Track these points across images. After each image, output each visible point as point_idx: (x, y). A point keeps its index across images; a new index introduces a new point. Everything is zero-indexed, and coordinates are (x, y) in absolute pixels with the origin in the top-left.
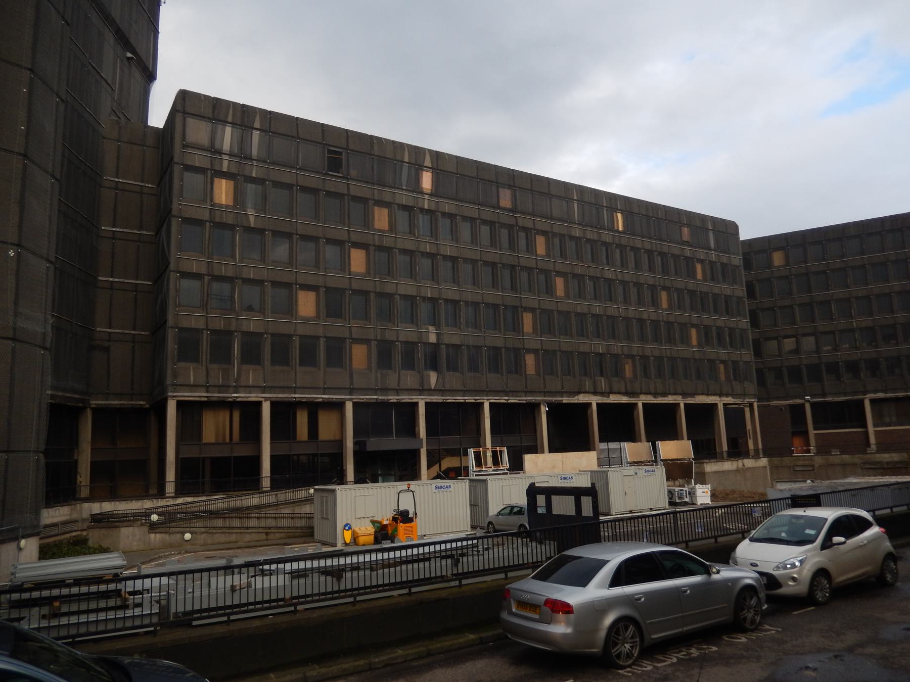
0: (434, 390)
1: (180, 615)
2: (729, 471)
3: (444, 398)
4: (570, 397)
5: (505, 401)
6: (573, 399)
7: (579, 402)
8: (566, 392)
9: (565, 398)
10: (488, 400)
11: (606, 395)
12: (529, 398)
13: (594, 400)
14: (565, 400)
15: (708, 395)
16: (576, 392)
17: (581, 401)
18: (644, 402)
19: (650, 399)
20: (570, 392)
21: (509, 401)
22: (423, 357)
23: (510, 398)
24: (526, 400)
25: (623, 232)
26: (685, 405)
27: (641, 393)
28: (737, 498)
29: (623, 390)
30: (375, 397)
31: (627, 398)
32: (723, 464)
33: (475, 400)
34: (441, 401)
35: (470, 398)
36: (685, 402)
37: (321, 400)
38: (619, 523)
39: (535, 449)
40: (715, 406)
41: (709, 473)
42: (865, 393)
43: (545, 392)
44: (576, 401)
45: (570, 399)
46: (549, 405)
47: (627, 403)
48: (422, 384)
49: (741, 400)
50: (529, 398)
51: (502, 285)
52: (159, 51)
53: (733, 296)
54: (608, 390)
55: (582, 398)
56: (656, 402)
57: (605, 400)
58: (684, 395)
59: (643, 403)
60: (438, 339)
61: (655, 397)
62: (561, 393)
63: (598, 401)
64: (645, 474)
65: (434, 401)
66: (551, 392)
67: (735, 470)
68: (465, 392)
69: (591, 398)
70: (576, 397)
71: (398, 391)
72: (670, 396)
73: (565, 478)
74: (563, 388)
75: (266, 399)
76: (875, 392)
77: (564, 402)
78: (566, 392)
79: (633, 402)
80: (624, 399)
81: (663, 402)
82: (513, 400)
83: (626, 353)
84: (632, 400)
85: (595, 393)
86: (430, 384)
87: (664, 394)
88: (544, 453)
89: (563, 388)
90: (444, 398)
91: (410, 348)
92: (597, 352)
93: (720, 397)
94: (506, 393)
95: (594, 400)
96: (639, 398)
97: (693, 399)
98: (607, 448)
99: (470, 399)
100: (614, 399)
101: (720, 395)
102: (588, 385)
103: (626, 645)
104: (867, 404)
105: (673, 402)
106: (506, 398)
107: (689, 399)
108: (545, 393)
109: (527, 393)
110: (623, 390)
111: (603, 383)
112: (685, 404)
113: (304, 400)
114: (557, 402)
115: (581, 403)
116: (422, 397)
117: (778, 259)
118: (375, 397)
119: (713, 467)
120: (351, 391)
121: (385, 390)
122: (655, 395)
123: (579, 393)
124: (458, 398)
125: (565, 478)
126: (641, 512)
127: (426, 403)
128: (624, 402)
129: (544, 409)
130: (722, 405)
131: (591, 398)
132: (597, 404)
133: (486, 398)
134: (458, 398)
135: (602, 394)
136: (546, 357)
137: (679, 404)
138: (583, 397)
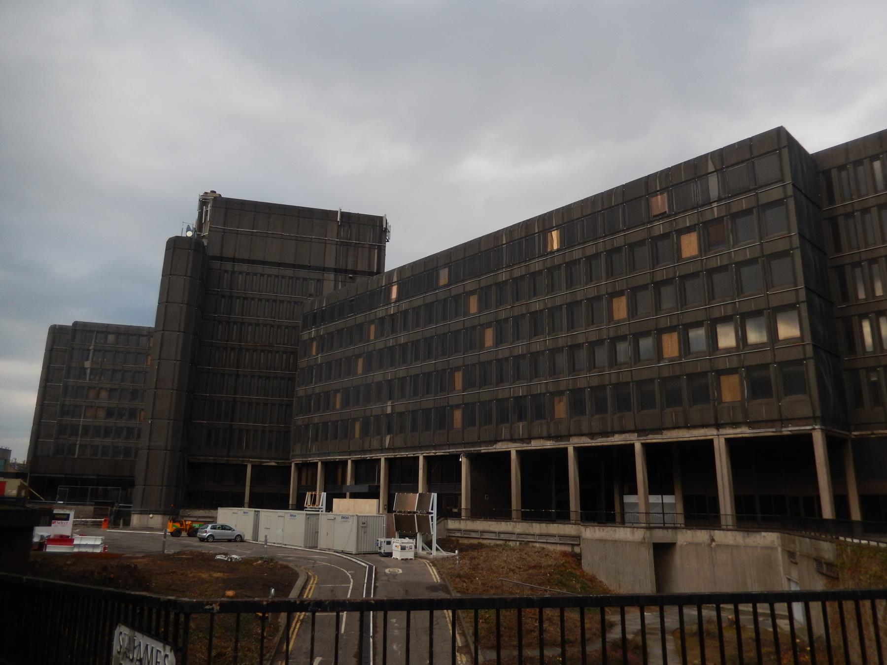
0: (388, 449)
1: (279, 566)
2: (624, 542)
3: (394, 454)
4: (488, 446)
5: (433, 454)
6: (491, 448)
7: (497, 450)
9: (482, 448)
10: (422, 454)
12: (451, 450)
13: (513, 448)
14: (484, 449)
15: (688, 427)
17: (499, 450)
18: (575, 445)
19: (586, 442)
21: (437, 454)
22: (711, 392)
23: (437, 451)
24: (449, 452)
26: (645, 446)
28: (551, 574)
29: (545, 434)
30: (360, 456)
31: (554, 442)
32: (615, 531)
33: (414, 454)
34: (393, 457)
35: (410, 453)
36: (643, 441)
37: (338, 460)
38: (718, 610)
39: (342, 496)
40: (709, 444)
41: (587, 539)
42: (568, 437)
43: (464, 443)
44: (494, 450)
45: (488, 448)
46: (469, 456)
47: (622, 445)
48: (382, 446)
49: (774, 430)
50: (451, 450)
51: (140, 419)
53: (396, 345)
54: (526, 436)
55: (500, 447)
56: (593, 444)
57: (525, 447)
58: (641, 432)
59: (574, 447)
60: (392, 410)
61: (592, 439)
62: (480, 444)
63: (517, 449)
64: (342, 520)
65: (389, 457)
66: (425, 446)
67: (639, 542)
68: (406, 449)
69: (509, 446)
70: (495, 446)
71: (370, 451)
72: (616, 436)
73: (344, 518)
74: (479, 438)
75: (350, 459)
76: (735, 424)
77: (482, 451)
79: (563, 446)
80: (549, 444)
81: (605, 444)
82: (440, 453)
83: (551, 390)
84: (561, 445)
85: (513, 440)
86: (385, 446)
87: (606, 434)
88: (346, 498)
89: (479, 438)
90: (394, 454)
92: (516, 395)
94: (435, 447)
95: (513, 448)
96: (569, 441)
98: (661, 502)
99: (410, 454)
100: (536, 445)
101: (718, 426)
102: (505, 433)
105: (623, 443)
106: (434, 451)
107: (651, 436)
108: (465, 445)
109: (450, 445)
110: (545, 434)
111: (521, 428)
112: (644, 445)
113: (332, 460)
114: (475, 452)
115: (498, 452)
116: (383, 455)
117: (555, 240)
118: (360, 456)
119: (597, 532)
120: (350, 453)
121: (364, 451)
122: (592, 435)
123: (496, 441)
124: (402, 454)
125: (344, 518)
126: (325, 550)
127: (385, 458)
128: (549, 447)
130: (722, 441)
131: (509, 446)
132: (517, 451)
133: (420, 452)
134: (402, 454)
135: (522, 440)
136: (468, 409)
137: (633, 445)
138: (502, 445)
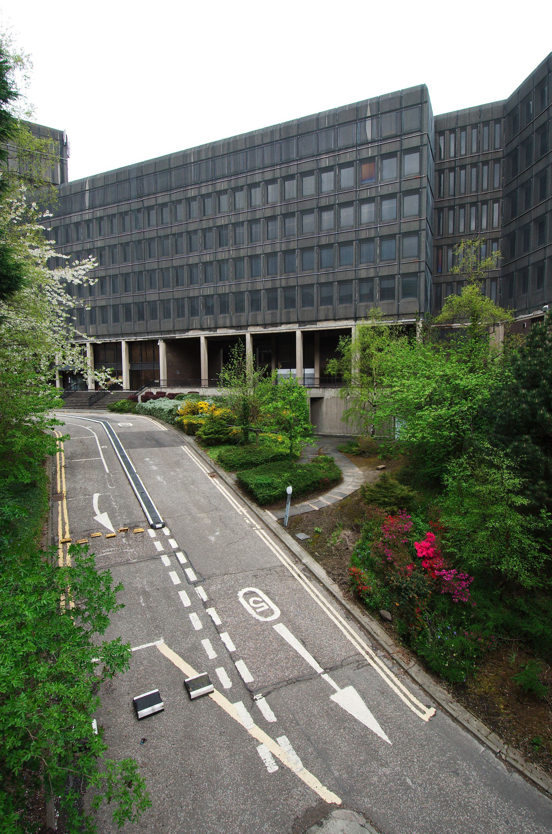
8: (177, 330)
11: (214, 329)
13: (202, 335)
14: (178, 336)
16: (185, 330)
18: (252, 333)
20: (183, 330)
25: (56, 240)
27: (248, 326)
36: (302, 330)
42: (246, 326)
43: (174, 331)
44: (187, 337)
46: (166, 341)
52: (69, 171)
55: (191, 334)
56: (265, 332)
58: (301, 323)
62: (174, 332)
77: (177, 338)
78: (177, 330)
80: (231, 332)
81: (274, 332)
85: (202, 329)
91: (140, 306)
93: (356, 321)
94: (136, 334)
95: (202, 335)
97: (314, 326)
99: (113, 340)
100: (221, 332)
103: (210, 522)
104: (124, 346)
108: (161, 332)
122: (265, 326)
123: (188, 330)
129: (162, 345)
135: (209, 329)
